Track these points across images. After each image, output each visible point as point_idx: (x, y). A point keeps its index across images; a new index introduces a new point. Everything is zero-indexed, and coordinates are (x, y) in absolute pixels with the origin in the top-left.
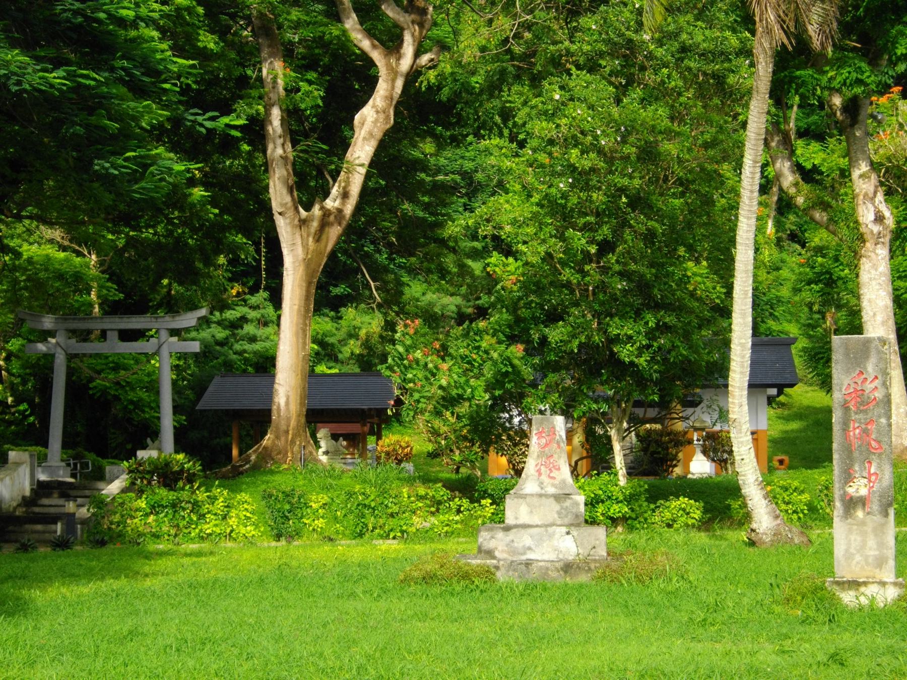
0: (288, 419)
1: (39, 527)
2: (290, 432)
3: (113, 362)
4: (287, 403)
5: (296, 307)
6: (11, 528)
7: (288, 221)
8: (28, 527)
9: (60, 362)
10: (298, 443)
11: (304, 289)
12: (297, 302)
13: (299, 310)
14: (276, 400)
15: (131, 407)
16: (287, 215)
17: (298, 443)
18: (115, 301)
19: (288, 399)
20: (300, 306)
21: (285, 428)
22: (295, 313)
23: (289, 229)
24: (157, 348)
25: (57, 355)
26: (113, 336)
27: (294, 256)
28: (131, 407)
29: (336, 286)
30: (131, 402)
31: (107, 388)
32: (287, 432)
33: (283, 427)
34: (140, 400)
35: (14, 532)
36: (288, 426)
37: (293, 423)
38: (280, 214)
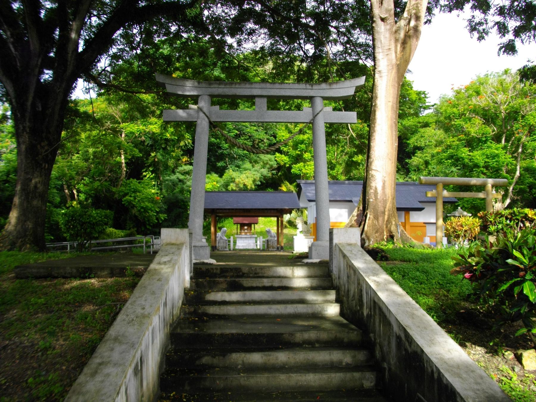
0: (385, 202)
1: (256, 358)
2: (386, 213)
3: (133, 189)
4: (384, 188)
5: (390, 104)
6: (206, 360)
7: (388, 27)
8: (239, 358)
9: (203, 126)
10: (394, 223)
11: (396, 89)
12: (391, 99)
13: (392, 106)
14: (373, 184)
15: (142, 210)
16: (388, 22)
17: (394, 223)
18: (138, 157)
19: (384, 184)
20: (393, 103)
21: (382, 209)
22: (390, 109)
23: (387, 35)
24: (311, 117)
25: (199, 122)
26: (262, 103)
27: (388, 60)
28: (142, 210)
29: (219, 162)
30: (142, 208)
31: (131, 200)
32: (384, 213)
33: (381, 209)
34: (147, 206)
35: (211, 367)
36: (385, 208)
37: (389, 205)
38: (383, 20)
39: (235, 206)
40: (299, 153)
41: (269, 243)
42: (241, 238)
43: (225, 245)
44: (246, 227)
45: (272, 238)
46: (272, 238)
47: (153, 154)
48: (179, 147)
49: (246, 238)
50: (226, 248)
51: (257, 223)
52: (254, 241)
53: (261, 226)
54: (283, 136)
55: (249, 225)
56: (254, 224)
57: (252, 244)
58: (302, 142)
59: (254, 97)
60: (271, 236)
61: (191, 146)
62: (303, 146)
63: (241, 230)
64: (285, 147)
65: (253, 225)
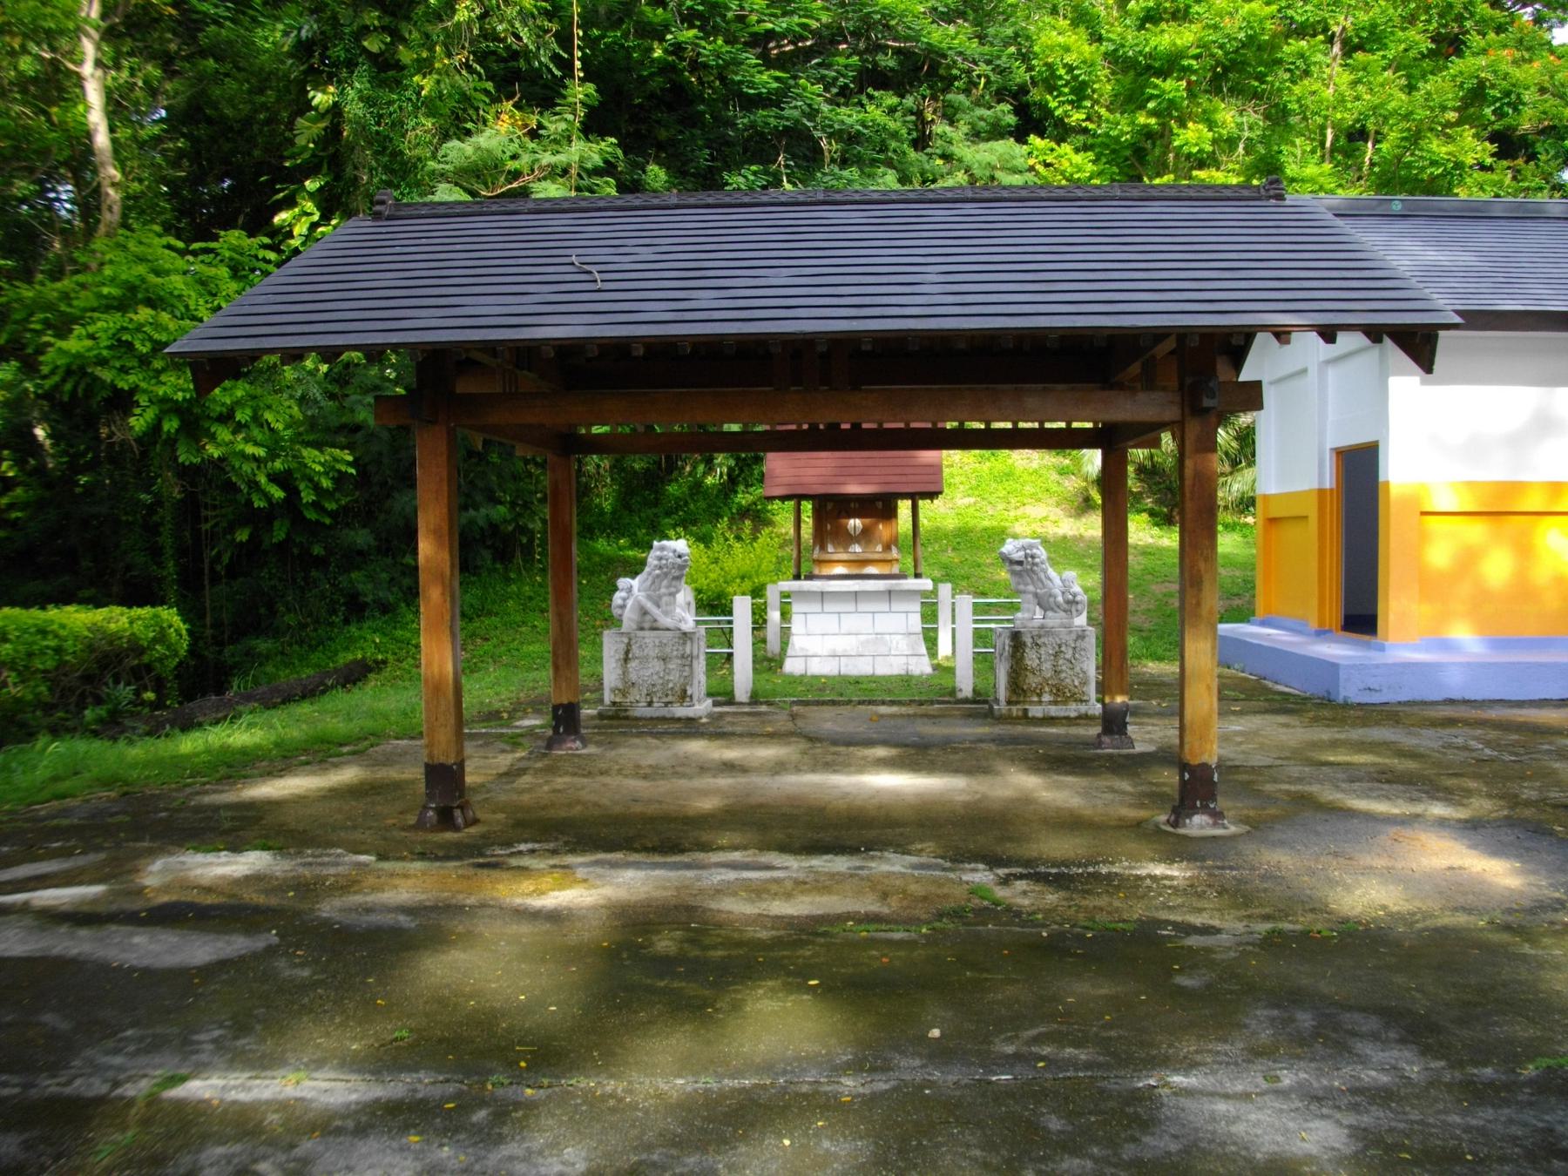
39: (657, 311)
40: (1153, 121)
41: (1031, 658)
42: (823, 596)
43: (675, 678)
44: (855, 523)
45: (1054, 620)
46: (1054, 620)
47: (321, 99)
48: (451, 40)
49: (856, 596)
50: (684, 697)
51: (932, 495)
52: (916, 622)
53: (962, 502)
54: (1067, 49)
55: (880, 507)
56: (914, 497)
57: (901, 644)
58: (1170, 65)
59: (974, 702)
60: (1045, 603)
61: (555, 58)
62: (1173, 87)
63: (821, 537)
64: (1076, 104)
65: (904, 507)
